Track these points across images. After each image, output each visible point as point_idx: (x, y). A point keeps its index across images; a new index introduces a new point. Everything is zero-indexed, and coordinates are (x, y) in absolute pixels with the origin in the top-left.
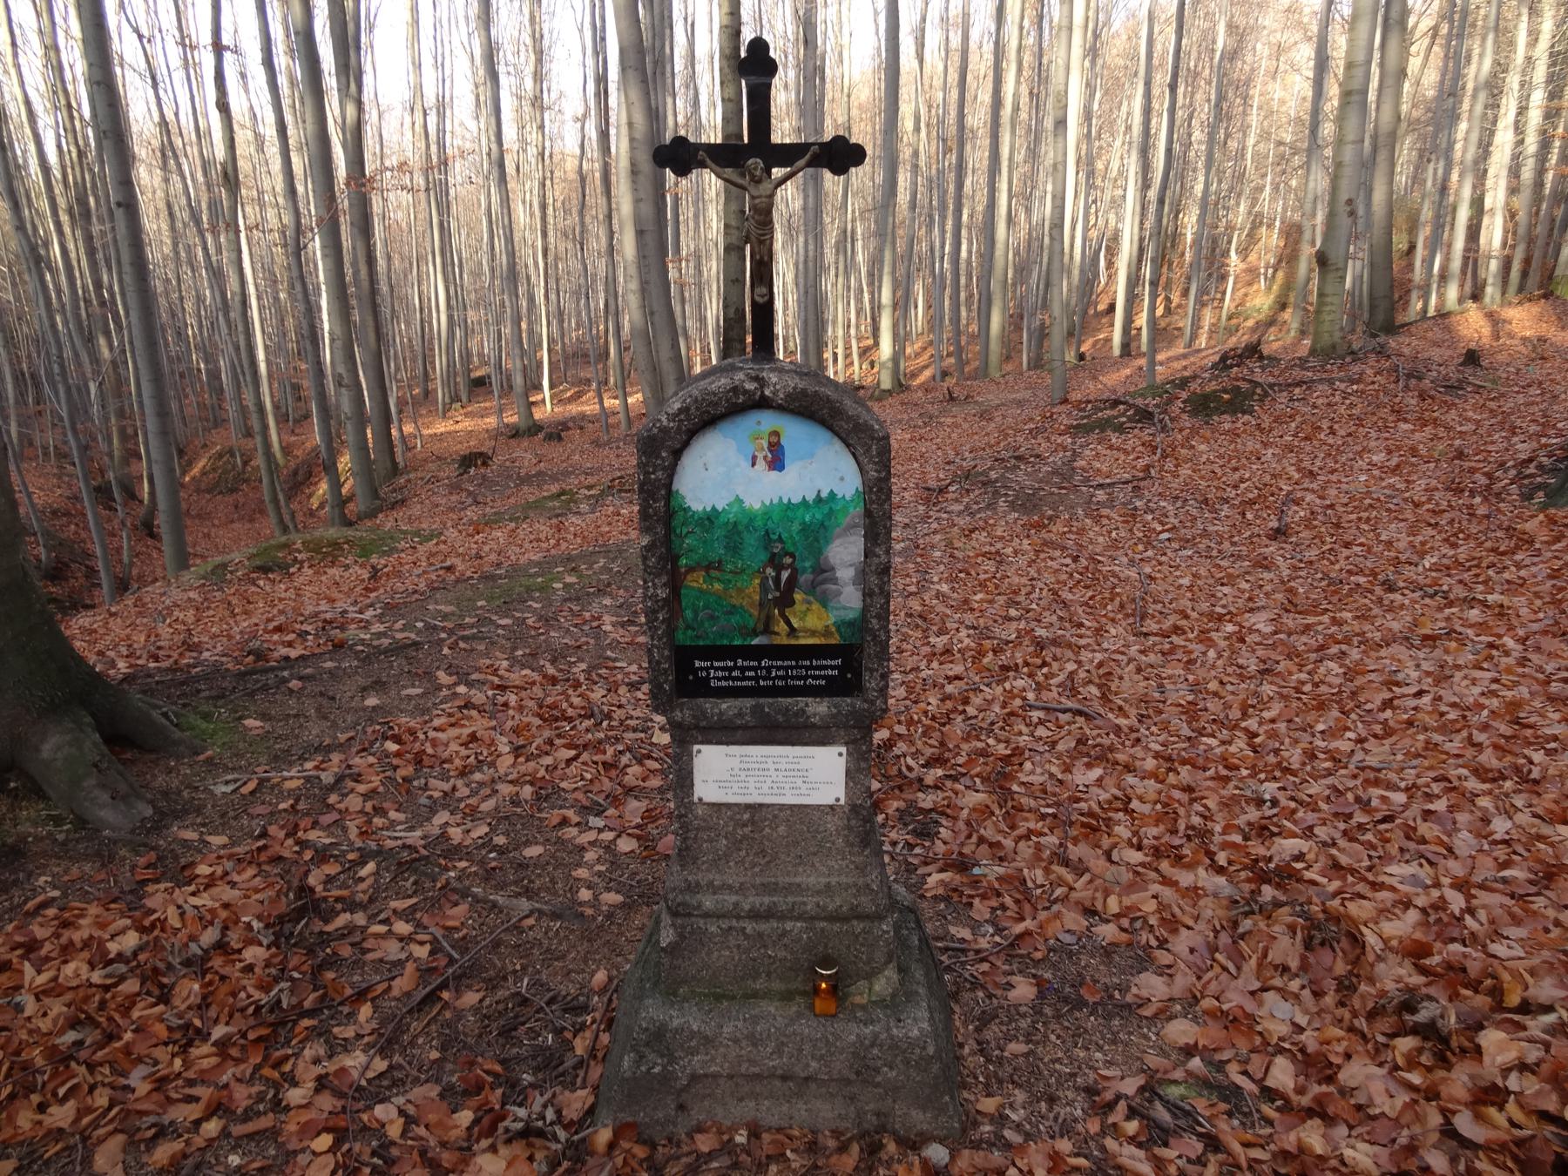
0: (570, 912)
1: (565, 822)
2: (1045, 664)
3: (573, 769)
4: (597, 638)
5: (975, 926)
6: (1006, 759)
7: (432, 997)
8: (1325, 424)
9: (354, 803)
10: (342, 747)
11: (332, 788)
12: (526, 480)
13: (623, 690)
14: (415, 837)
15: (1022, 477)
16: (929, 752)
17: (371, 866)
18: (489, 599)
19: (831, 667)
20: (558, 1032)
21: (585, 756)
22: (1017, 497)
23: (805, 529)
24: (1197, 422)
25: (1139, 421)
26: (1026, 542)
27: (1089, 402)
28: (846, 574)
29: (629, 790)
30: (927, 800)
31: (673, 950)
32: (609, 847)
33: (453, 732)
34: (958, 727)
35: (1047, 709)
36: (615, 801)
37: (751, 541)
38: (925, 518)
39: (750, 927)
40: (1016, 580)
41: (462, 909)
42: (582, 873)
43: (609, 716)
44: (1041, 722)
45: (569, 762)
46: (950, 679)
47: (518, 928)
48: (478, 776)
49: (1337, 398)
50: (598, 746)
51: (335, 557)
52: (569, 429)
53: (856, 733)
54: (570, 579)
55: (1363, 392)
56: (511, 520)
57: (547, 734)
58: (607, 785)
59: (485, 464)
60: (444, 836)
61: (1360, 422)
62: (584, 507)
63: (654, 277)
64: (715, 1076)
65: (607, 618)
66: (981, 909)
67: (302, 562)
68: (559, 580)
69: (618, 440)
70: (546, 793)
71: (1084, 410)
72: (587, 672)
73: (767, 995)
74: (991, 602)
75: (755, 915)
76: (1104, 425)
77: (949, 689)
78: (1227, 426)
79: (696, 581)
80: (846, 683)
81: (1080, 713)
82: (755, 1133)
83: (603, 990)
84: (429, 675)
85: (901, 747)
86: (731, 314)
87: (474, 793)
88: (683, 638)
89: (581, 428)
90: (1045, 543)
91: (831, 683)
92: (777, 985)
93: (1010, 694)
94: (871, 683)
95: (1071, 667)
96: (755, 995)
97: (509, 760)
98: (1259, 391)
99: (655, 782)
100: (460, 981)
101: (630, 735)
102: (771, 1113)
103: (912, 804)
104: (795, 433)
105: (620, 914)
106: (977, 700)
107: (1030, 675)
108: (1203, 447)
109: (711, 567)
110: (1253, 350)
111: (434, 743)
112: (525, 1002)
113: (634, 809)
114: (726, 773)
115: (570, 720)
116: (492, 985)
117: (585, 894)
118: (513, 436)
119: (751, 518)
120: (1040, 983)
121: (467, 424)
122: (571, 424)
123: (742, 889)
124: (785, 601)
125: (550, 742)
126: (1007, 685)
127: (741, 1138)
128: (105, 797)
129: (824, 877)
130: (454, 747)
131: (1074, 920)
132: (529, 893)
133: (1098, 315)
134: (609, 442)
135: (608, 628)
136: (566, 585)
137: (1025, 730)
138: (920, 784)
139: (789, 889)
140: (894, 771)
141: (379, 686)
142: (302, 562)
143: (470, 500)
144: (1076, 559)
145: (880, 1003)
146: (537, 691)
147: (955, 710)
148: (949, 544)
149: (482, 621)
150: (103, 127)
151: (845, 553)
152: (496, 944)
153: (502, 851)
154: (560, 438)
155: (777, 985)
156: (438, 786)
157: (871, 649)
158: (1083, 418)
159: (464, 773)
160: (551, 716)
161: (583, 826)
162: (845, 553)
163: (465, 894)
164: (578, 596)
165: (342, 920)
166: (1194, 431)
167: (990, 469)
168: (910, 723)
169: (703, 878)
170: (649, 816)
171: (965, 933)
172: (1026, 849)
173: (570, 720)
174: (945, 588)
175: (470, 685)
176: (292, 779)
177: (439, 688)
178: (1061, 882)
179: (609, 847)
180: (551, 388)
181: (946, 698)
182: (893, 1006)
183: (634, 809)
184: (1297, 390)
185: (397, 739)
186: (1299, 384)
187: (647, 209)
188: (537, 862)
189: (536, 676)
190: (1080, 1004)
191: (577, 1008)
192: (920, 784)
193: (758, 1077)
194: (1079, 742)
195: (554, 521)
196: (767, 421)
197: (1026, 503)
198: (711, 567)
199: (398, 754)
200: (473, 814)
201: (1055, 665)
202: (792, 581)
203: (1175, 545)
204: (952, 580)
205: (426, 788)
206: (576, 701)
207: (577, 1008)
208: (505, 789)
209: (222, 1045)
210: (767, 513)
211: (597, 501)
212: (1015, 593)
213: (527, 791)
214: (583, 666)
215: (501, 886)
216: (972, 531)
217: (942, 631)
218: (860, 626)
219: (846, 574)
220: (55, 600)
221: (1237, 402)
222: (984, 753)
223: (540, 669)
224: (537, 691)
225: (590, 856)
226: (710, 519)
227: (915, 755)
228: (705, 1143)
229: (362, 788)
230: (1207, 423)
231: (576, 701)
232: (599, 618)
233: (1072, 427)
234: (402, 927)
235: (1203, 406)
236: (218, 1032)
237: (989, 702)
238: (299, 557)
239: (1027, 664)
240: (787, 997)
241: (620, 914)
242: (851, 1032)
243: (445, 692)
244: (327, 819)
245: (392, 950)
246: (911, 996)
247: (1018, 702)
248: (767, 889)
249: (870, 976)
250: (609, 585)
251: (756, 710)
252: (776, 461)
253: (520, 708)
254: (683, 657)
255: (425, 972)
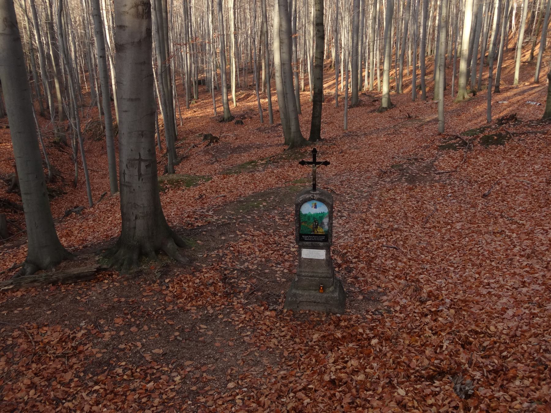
0: (275, 281)
1: (272, 266)
2: (392, 235)
3: (273, 255)
4: (274, 223)
5: (355, 288)
6: (373, 258)
7: (253, 293)
8: (527, 151)
9: (228, 260)
10: (221, 248)
11: (222, 257)
12: (234, 150)
13: (283, 237)
14: (242, 267)
15: (414, 169)
16: (355, 255)
17: (236, 272)
18: (243, 210)
19: (323, 238)
20: (276, 299)
21: (275, 253)
22: (409, 177)
23: (320, 217)
24: (482, 148)
25: (462, 146)
26: (405, 195)
27: (448, 135)
28: (326, 224)
29: (286, 260)
30: (352, 266)
31: (297, 281)
32: (282, 271)
33: (245, 246)
34: (365, 249)
35: (388, 247)
36: (283, 262)
37: (311, 219)
38: (376, 184)
39: (310, 278)
40: (396, 209)
41: (255, 280)
42: (277, 275)
43: (280, 244)
44: (385, 250)
45: (272, 254)
46: (366, 238)
47: (266, 283)
48: (252, 256)
49: (536, 140)
50: (278, 251)
51: (179, 187)
52: (245, 118)
53: (327, 248)
54: (265, 204)
55: (546, 138)
56: (235, 173)
57: (266, 247)
58: (281, 259)
59: (216, 141)
60: (248, 267)
61: (539, 151)
62: (260, 168)
63: (288, 80)
64: (304, 301)
65: (277, 217)
66: (357, 285)
67: (169, 188)
68: (262, 204)
69: (269, 129)
70: (268, 260)
71: (445, 139)
72: (273, 232)
73: (312, 290)
74: (386, 216)
75: (311, 276)
76: (451, 147)
77: (365, 241)
78: (493, 150)
79: (303, 224)
80: (326, 240)
81: (395, 248)
82: (309, 311)
83: (283, 294)
84: (234, 232)
85: (349, 254)
86: (317, 90)
87: (252, 259)
88: (301, 232)
89: (251, 118)
90: (411, 196)
91: (323, 240)
92: (314, 288)
93: (380, 243)
94: (329, 240)
95: (398, 236)
96: (310, 290)
97: (258, 253)
98: (508, 136)
99: (291, 259)
100: (258, 290)
101: (285, 248)
102: (312, 308)
103: (348, 266)
104: (318, 203)
105: (285, 283)
106: (371, 244)
107: (387, 238)
108: (481, 158)
109: (305, 222)
110: (513, 117)
111: (241, 248)
112: (269, 294)
113: (287, 264)
114: (307, 253)
115: (271, 244)
116: (263, 292)
117: (278, 279)
118: (221, 122)
119: (311, 215)
120: (364, 297)
121: (199, 113)
122: (246, 116)
123: (309, 272)
124: (317, 227)
125: (267, 249)
126: (379, 241)
127: (307, 312)
128: (180, 256)
129: (323, 271)
130: (245, 249)
131: (375, 288)
132: (267, 278)
133: (508, 50)
134: (265, 130)
135: (277, 220)
136: (264, 206)
137: (380, 251)
138: (352, 262)
139: (316, 273)
140: (345, 259)
141: (223, 234)
142: (169, 188)
143: (214, 159)
144: (418, 202)
145: (330, 292)
146: (262, 237)
147: (364, 246)
148: (381, 195)
149: (243, 217)
150: (97, 30)
151: (326, 221)
152: (262, 286)
153: (260, 271)
154: (242, 123)
155: (314, 288)
156: (244, 258)
157: (329, 235)
158: (444, 142)
159: (249, 255)
160: (267, 243)
161: (277, 267)
162: (326, 221)
163: (255, 277)
164: (267, 209)
165: (233, 280)
166: (481, 152)
167: (405, 164)
168: (353, 248)
169: (303, 270)
170: (290, 266)
171: (353, 289)
172: (369, 275)
173: (271, 244)
174: (374, 210)
175: (245, 234)
176: (214, 254)
177: (238, 235)
178: (374, 281)
179: (282, 271)
180: (236, 92)
181: (363, 243)
182: (333, 292)
183: (287, 264)
184: (523, 136)
185: (232, 247)
186: (524, 134)
187: (286, 56)
188: (268, 273)
189: (260, 233)
190: (370, 300)
191: (279, 296)
192: (352, 262)
193: (310, 302)
194: (392, 255)
195: (250, 174)
196: (314, 202)
197: (412, 180)
198: (305, 222)
199: (234, 250)
200: (253, 263)
201: (394, 236)
202: (318, 225)
203: (451, 198)
204: (377, 208)
205: (241, 258)
206: (272, 240)
207: (279, 296)
208: (259, 259)
209: (220, 296)
210: (314, 214)
211: (265, 166)
212: (394, 213)
213: (263, 259)
214: (272, 231)
215: (261, 277)
216: (389, 190)
217: (368, 225)
218: (328, 231)
219: (326, 224)
220: (54, 191)
221: (499, 140)
222: (368, 256)
223: (261, 231)
224: (262, 237)
225: (278, 272)
226: (306, 215)
227: (351, 256)
228: (301, 312)
229: (229, 257)
230: (486, 148)
231: (272, 240)
232: (274, 217)
233: (439, 146)
234: (244, 282)
235: (487, 141)
236: (219, 294)
237: (374, 244)
238: (168, 186)
239: (387, 235)
240: (316, 290)
241: (285, 283)
242: (325, 295)
243: (239, 236)
244: (224, 263)
245: (244, 286)
246: (336, 291)
247: (381, 245)
248: (313, 272)
249: (329, 287)
250: (276, 206)
251: (312, 244)
252: (316, 207)
253: (259, 241)
254: (301, 235)
255: (251, 289)
